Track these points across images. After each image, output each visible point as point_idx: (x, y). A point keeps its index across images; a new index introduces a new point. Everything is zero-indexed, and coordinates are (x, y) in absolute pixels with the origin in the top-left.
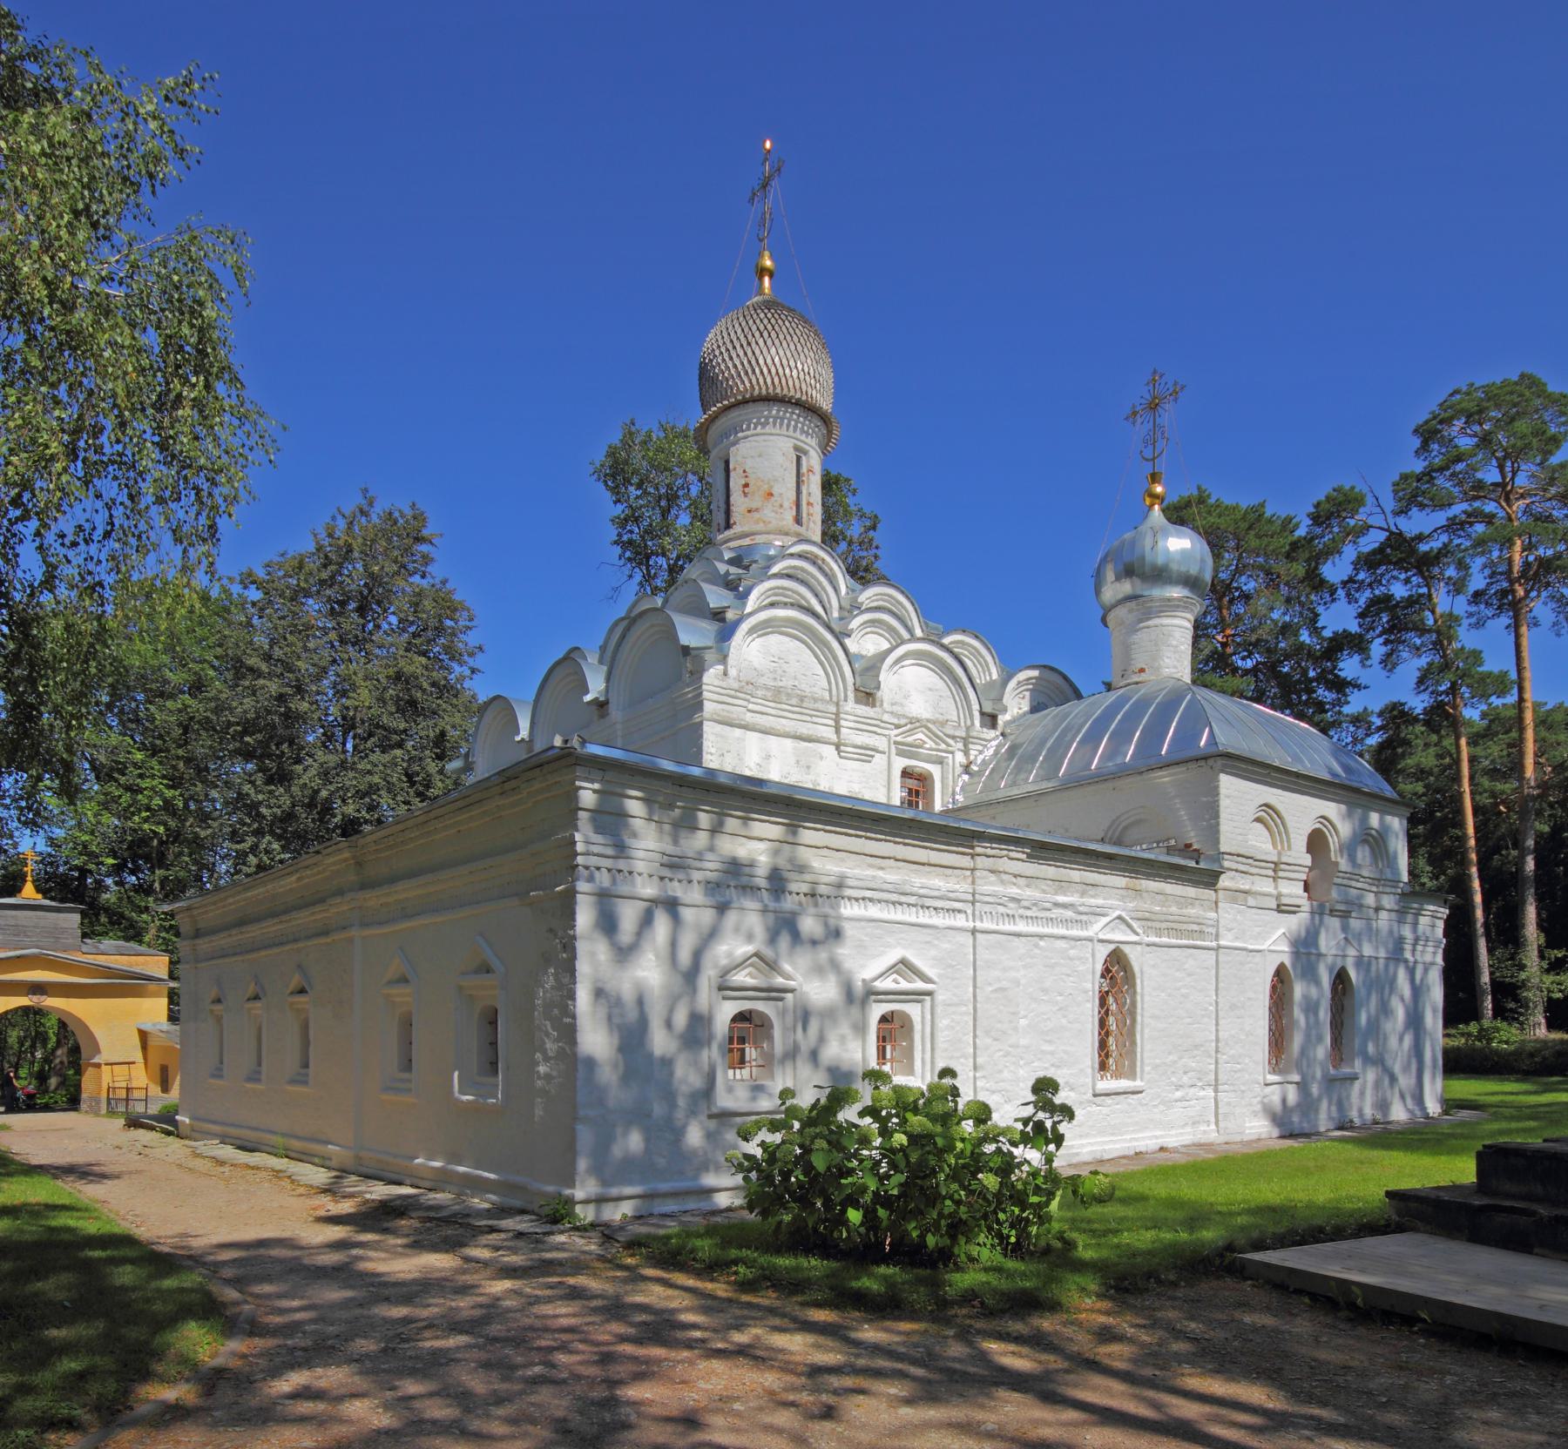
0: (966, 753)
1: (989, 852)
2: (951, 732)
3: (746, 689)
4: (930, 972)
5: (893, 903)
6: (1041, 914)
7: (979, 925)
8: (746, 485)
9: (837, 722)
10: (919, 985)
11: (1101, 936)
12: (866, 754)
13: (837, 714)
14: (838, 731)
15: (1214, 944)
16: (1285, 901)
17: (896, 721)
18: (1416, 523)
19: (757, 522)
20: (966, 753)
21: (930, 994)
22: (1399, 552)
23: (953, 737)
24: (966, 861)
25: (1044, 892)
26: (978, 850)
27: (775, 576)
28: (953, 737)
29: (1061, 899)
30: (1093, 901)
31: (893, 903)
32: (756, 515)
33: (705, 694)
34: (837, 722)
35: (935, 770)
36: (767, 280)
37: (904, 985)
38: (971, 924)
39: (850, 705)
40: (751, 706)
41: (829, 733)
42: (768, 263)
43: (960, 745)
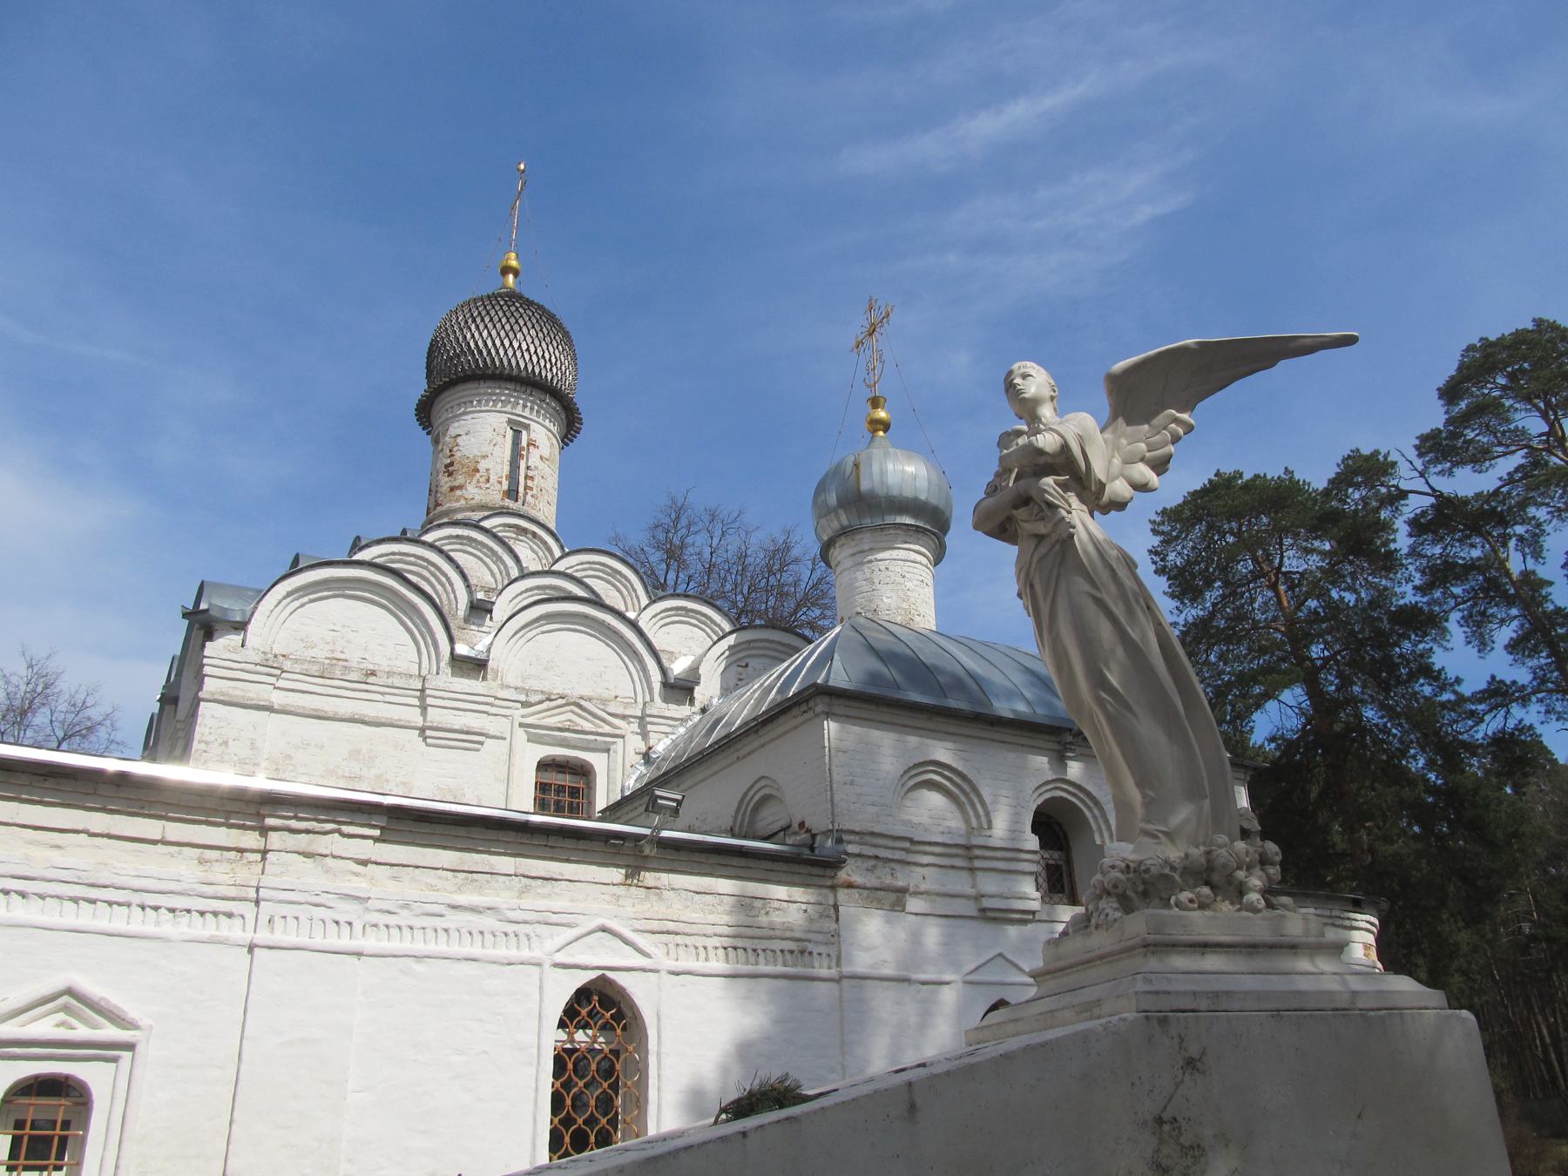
0: (645, 735)
1: (293, 824)
2: (619, 711)
3: (273, 665)
4: (132, 1013)
5: (75, 900)
6: (419, 922)
7: (263, 936)
8: (452, 464)
9: (422, 698)
10: (110, 1032)
11: (561, 958)
12: (471, 739)
13: (423, 690)
14: (424, 708)
15: (833, 972)
16: (986, 903)
17: (523, 698)
18: (1466, 483)
19: (458, 500)
20: (645, 735)
21: (130, 1047)
22: (1446, 516)
23: (624, 717)
24: (251, 839)
25: (432, 887)
26: (270, 821)
27: (431, 546)
28: (624, 717)
29: (462, 899)
30: (542, 904)
31: (75, 900)
32: (459, 493)
33: (207, 670)
34: (422, 698)
35: (597, 760)
36: (511, 277)
37: (82, 1032)
38: (248, 936)
39: (659, 706)
40: (281, 683)
41: (415, 716)
42: (514, 263)
43: (635, 727)
